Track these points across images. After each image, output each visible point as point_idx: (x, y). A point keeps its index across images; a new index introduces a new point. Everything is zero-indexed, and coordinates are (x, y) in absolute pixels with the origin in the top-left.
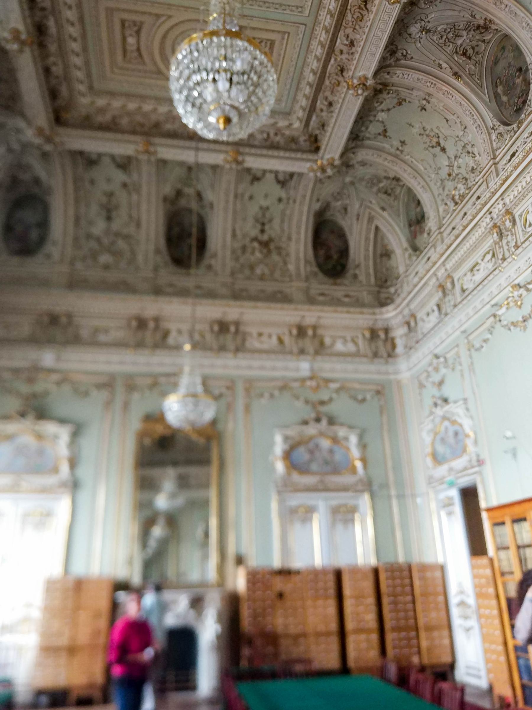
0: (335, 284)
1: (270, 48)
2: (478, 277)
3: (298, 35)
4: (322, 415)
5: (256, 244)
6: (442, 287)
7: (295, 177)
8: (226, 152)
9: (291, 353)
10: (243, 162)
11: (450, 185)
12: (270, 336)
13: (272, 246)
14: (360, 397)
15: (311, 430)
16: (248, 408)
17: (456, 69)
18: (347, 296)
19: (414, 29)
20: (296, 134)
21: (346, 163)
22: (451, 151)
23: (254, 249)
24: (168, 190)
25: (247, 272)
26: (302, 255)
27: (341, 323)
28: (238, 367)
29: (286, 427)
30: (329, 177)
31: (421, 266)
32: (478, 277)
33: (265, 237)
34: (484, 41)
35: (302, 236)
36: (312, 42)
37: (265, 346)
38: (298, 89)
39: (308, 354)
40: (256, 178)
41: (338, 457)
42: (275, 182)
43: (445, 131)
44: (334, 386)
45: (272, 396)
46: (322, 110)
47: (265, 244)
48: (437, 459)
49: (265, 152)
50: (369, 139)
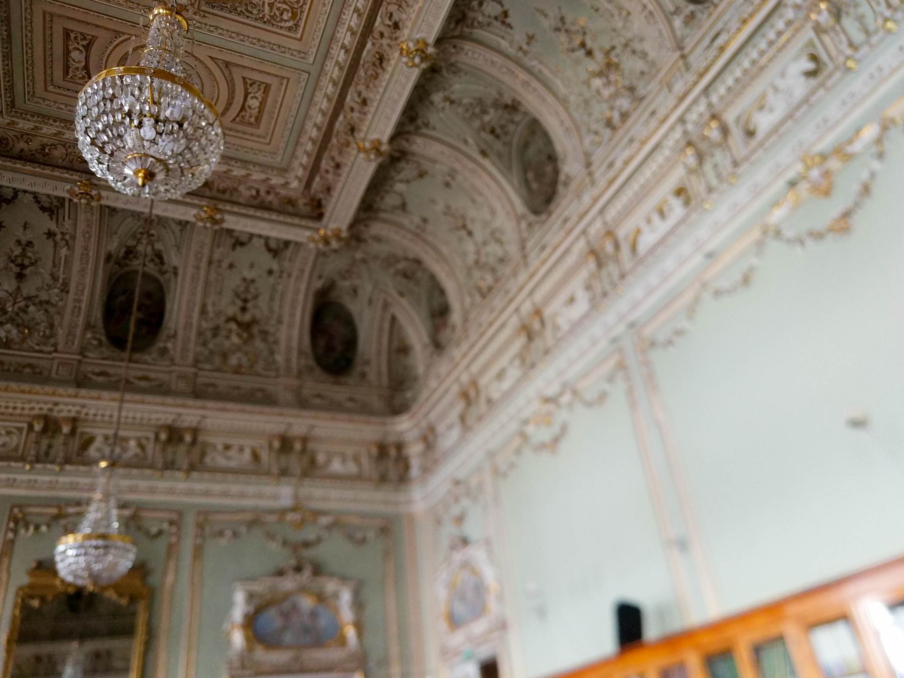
0: (337, 383)
1: (264, 92)
2: (506, 384)
3: (300, 82)
4: (305, 563)
5: (233, 326)
6: (465, 395)
7: (292, 247)
8: (200, 207)
9: (268, 473)
10: (222, 220)
11: (477, 274)
12: (241, 450)
13: (255, 330)
14: (359, 535)
15: (288, 584)
16: (198, 552)
17: (484, 147)
18: (351, 399)
19: (437, 97)
20: (292, 194)
21: (356, 235)
22: (479, 235)
23: (230, 331)
24: (113, 245)
25: (217, 360)
26: (295, 344)
27: (341, 436)
28: (190, 493)
29: (253, 579)
30: (335, 251)
31: (443, 367)
32: (506, 384)
33: (247, 318)
34: (513, 122)
35: (298, 319)
36: (316, 93)
37: (233, 464)
38: (297, 143)
39: (291, 475)
40: (239, 242)
41: (323, 622)
42: (264, 249)
43: (472, 213)
44: (324, 520)
45: (235, 534)
46: (327, 172)
47: (246, 327)
48: (454, 622)
49: (251, 212)
50: (384, 211)
